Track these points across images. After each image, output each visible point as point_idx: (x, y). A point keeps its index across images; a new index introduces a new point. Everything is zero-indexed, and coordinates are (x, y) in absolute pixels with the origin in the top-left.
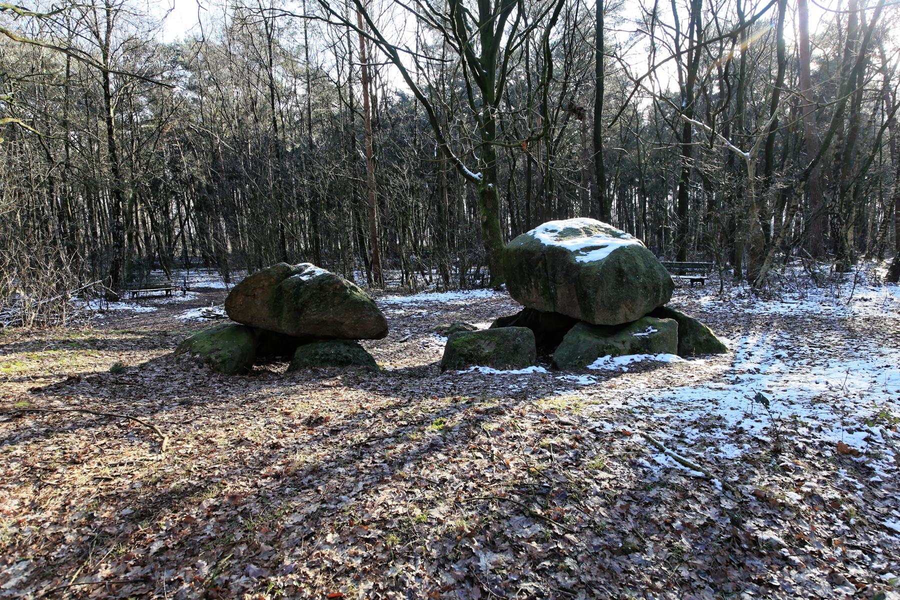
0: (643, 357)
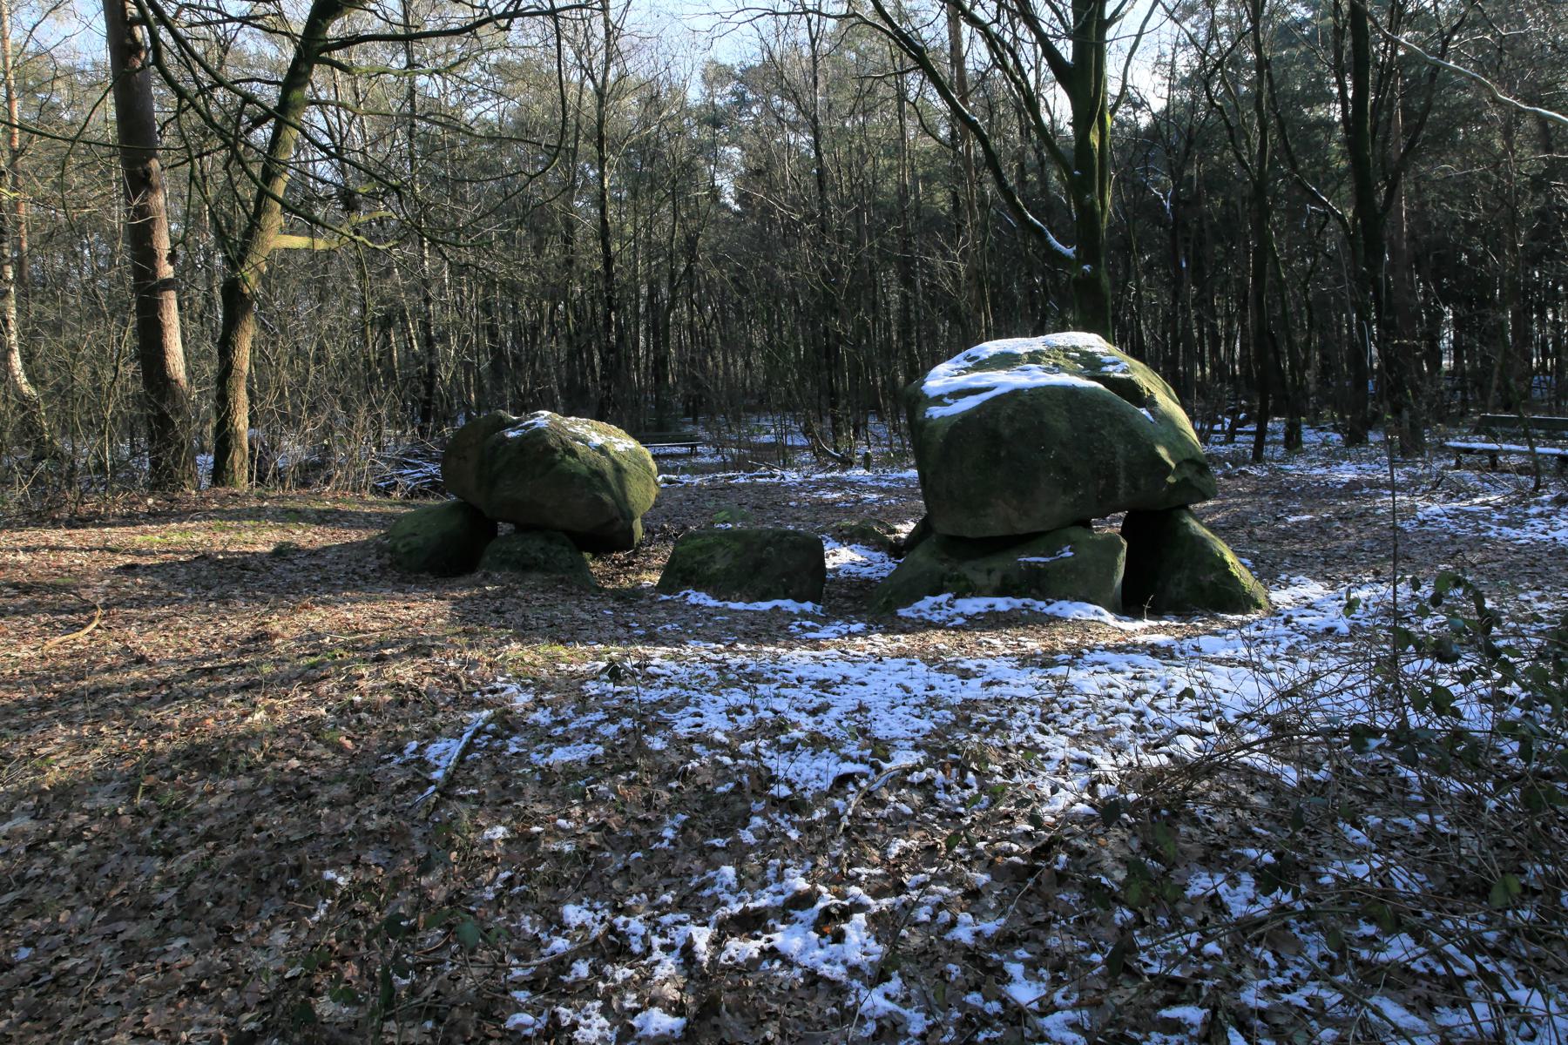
0: (1018, 603)
